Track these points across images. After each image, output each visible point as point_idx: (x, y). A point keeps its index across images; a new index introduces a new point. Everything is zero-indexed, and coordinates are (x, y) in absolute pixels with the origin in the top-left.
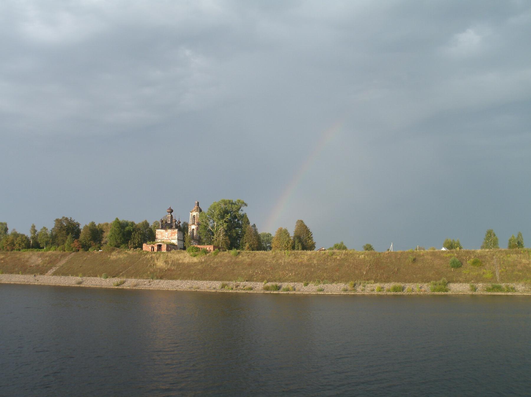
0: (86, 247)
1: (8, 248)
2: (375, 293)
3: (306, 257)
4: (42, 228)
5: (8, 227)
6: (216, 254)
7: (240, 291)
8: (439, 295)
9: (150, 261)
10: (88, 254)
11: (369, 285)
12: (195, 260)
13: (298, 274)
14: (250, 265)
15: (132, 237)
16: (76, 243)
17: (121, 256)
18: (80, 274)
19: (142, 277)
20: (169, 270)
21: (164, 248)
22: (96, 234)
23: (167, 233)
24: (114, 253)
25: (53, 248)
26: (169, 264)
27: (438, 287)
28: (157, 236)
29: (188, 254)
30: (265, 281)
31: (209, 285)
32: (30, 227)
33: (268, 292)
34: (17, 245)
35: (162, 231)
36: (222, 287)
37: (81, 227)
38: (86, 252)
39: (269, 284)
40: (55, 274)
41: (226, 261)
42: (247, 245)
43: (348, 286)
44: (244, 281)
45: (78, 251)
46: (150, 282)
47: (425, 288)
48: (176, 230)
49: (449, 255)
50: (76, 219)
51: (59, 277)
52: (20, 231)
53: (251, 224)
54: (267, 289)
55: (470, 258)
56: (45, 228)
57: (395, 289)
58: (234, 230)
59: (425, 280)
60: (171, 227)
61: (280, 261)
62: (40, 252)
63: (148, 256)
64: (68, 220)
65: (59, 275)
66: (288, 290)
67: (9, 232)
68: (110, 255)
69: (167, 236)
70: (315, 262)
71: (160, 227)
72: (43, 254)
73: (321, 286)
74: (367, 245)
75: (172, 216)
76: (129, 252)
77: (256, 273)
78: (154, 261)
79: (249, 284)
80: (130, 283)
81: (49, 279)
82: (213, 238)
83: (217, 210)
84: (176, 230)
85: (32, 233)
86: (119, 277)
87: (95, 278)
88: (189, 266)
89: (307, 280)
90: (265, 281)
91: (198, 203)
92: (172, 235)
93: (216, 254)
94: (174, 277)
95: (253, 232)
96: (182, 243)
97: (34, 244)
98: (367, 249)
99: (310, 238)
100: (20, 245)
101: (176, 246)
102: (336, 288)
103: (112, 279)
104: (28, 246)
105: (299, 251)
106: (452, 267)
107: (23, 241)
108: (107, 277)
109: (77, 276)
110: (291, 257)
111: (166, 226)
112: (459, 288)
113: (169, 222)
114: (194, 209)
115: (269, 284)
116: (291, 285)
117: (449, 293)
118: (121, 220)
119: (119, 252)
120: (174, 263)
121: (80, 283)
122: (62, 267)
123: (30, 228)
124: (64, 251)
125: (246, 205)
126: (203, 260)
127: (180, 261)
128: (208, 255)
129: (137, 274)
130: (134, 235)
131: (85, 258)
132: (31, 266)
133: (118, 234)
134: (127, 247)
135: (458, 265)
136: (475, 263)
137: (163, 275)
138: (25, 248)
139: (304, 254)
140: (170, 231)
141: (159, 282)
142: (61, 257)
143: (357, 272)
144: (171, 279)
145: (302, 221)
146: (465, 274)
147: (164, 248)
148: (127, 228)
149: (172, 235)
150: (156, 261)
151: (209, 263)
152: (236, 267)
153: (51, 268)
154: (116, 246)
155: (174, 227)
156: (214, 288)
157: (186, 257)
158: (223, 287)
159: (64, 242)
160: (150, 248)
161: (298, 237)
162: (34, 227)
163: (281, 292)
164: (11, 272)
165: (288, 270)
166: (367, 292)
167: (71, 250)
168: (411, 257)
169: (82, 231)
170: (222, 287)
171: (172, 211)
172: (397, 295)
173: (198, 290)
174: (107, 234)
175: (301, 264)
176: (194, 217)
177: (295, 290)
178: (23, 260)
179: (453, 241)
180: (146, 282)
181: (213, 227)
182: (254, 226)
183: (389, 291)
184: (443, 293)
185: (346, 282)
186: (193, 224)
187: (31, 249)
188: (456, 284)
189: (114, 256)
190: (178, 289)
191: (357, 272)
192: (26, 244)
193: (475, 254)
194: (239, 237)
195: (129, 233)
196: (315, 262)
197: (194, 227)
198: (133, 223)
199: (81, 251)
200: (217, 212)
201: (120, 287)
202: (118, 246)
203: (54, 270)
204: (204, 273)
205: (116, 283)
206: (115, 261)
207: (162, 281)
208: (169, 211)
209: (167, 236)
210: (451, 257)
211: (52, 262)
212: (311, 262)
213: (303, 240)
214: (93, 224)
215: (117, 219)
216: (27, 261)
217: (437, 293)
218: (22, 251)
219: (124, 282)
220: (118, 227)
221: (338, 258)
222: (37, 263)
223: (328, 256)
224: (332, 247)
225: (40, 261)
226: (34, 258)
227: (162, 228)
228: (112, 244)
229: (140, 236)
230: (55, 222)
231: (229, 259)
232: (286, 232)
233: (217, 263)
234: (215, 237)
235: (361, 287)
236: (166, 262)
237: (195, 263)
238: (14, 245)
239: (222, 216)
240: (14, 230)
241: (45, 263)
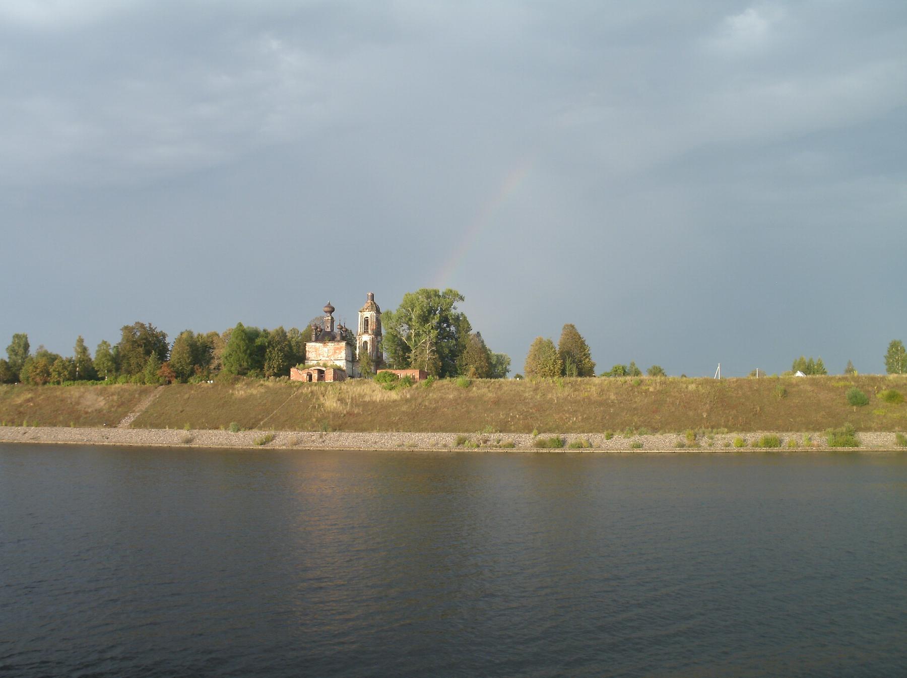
0: (183, 376)
1: (38, 379)
2: (734, 449)
3: (594, 389)
4: (100, 342)
5: (30, 341)
6: (429, 385)
7: (494, 450)
8: (843, 453)
9: (310, 400)
10: (191, 389)
11: (719, 436)
12: (394, 395)
13: (588, 418)
14: (497, 402)
15: (267, 357)
16: (166, 370)
17: (254, 391)
18: (187, 426)
19: (303, 429)
20: (349, 414)
21: (329, 376)
22: (199, 353)
23: (326, 349)
24: (238, 386)
25: (122, 379)
26: (346, 404)
27: (841, 440)
28: (308, 355)
29: (378, 386)
30: (535, 431)
31: (433, 440)
32: (75, 342)
33: (545, 451)
34: (55, 375)
35: (318, 345)
36: (459, 444)
37: (170, 340)
38: (185, 385)
39: (543, 437)
40: (137, 424)
41: (451, 397)
42: (472, 369)
43: (683, 438)
44: (496, 431)
45: (170, 382)
46: (321, 437)
47: (818, 441)
48: (343, 344)
49: (842, 383)
50: (159, 327)
51: (147, 432)
52: (52, 349)
53: (473, 332)
54: (541, 444)
55: (879, 389)
56: (105, 343)
57: (768, 443)
58: (447, 345)
59: (811, 426)
60: (333, 339)
61: (550, 396)
62: (99, 387)
63: (305, 390)
64: (145, 328)
65: (145, 426)
66: (580, 446)
67: (33, 351)
68: (233, 389)
69: (325, 355)
70: (613, 397)
71: (313, 339)
72: (105, 389)
73: (636, 438)
74: (654, 368)
75: (332, 318)
76: (267, 383)
77: (513, 418)
78: (318, 399)
79: (507, 438)
80: (284, 439)
81: (125, 435)
82: (409, 357)
83: (418, 308)
84: (343, 344)
85: (78, 353)
86: (260, 429)
87: (215, 431)
88: (384, 407)
89: (609, 427)
90: (535, 431)
91: (373, 296)
92: (335, 352)
93: (429, 385)
94: (346, 426)
95: (480, 345)
96: (350, 365)
97: (85, 372)
98: (655, 374)
99: (587, 356)
100: (59, 374)
101: (344, 371)
102: (664, 443)
103: (247, 432)
104: (74, 377)
105: (573, 379)
106: (854, 404)
107: (65, 368)
108: (239, 430)
109: (181, 428)
110: (566, 389)
111: (324, 336)
112: (873, 441)
113: (329, 330)
115: (543, 437)
116: (583, 437)
117: (862, 448)
118: (245, 326)
119: (247, 384)
120: (355, 402)
121: (188, 441)
122: (146, 412)
123: (74, 343)
124: (144, 383)
125: (462, 299)
126: (408, 396)
127: (367, 399)
128: (414, 386)
129: (291, 423)
130: (268, 354)
131: (186, 396)
132: (87, 413)
133: (245, 351)
134: (262, 374)
135: (860, 401)
136: (892, 397)
137: (341, 423)
138: (68, 380)
139: (587, 384)
140: (331, 345)
141: (339, 436)
142: (140, 394)
143: (691, 413)
144: (356, 430)
145: (572, 326)
146: (878, 416)
147: (329, 376)
148: (258, 341)
149: (335, 352)
150: (322, 398)
151: (420, 400)
152: (472, 407)
153: (125, 415)
154: (239, 374)
155: (338, 338)
156: (445, 446)
157: (374, 391)
158: (461, 442)
159: (140, 368)
160: (305, 375)
161: (565, 354)
162: (81, 341)
163: (567, 450)
164: (52, 422)
165: (568, 411)
166: (719, 448)
167: (157, 381)
168: (781, 388)
169: (170, 347)
170: (459, 444)
171: (333, 310)
172: (773, 453)
173: (416, 450)
174: (220, 352)
175: (589, 402)
176: (366, 321)
177: (591, 446)
178: (69, 401)
179: (811, 360)
180: (316, 436)
181: (409, 338)
182: (478, 334)
183: (756, 445)
184: (851, 449)
185: (678, 431)
186: (366, 332)
187: (80, 381)
188: (869, 434)
189: (241, 391)
190: (376, 447)
191: (691, 413)
192: (70, 373)
193: (887, 382)
194: (454, 354)
195: (262, 349)
196: (613, 397)
197: (367, 338)
198: (282, 334)
200: (417, 311)
201: (269, 447)
202: (243, 373)
203: (132, 417)
204: (417, 418)
205: (258, 440)
206: (245, 400)
207: (345, 434)
208: (327, 309)
209: (325, 355)
210: (846, 387)
211: (125, 405)
212: (604, 397)
213: (573, 359)
214: (190, 334)
215: (240, 325)
216: (78, 403)
217: (840, 449)
218: (62, 385)
219: (274, 437)
220: (244, 340)
221: (651, 389)
222: (97, 406)
223: (633, 387)
224: (609, 371)
225: (101, 403)
226: (90, 397)
227: (317, 340)
228: (233, 369)
229: (281, 354)
230: (121, 332)
231: (456, 393)
232: (550, 344)
233: (437, 402)
234: (412, 355)
235: (706, 439)
236: (341, 400)
237: (395, 401)
238: (49, 374)
239: (424, 319)
240: (41, 347)
241: (113, 406)
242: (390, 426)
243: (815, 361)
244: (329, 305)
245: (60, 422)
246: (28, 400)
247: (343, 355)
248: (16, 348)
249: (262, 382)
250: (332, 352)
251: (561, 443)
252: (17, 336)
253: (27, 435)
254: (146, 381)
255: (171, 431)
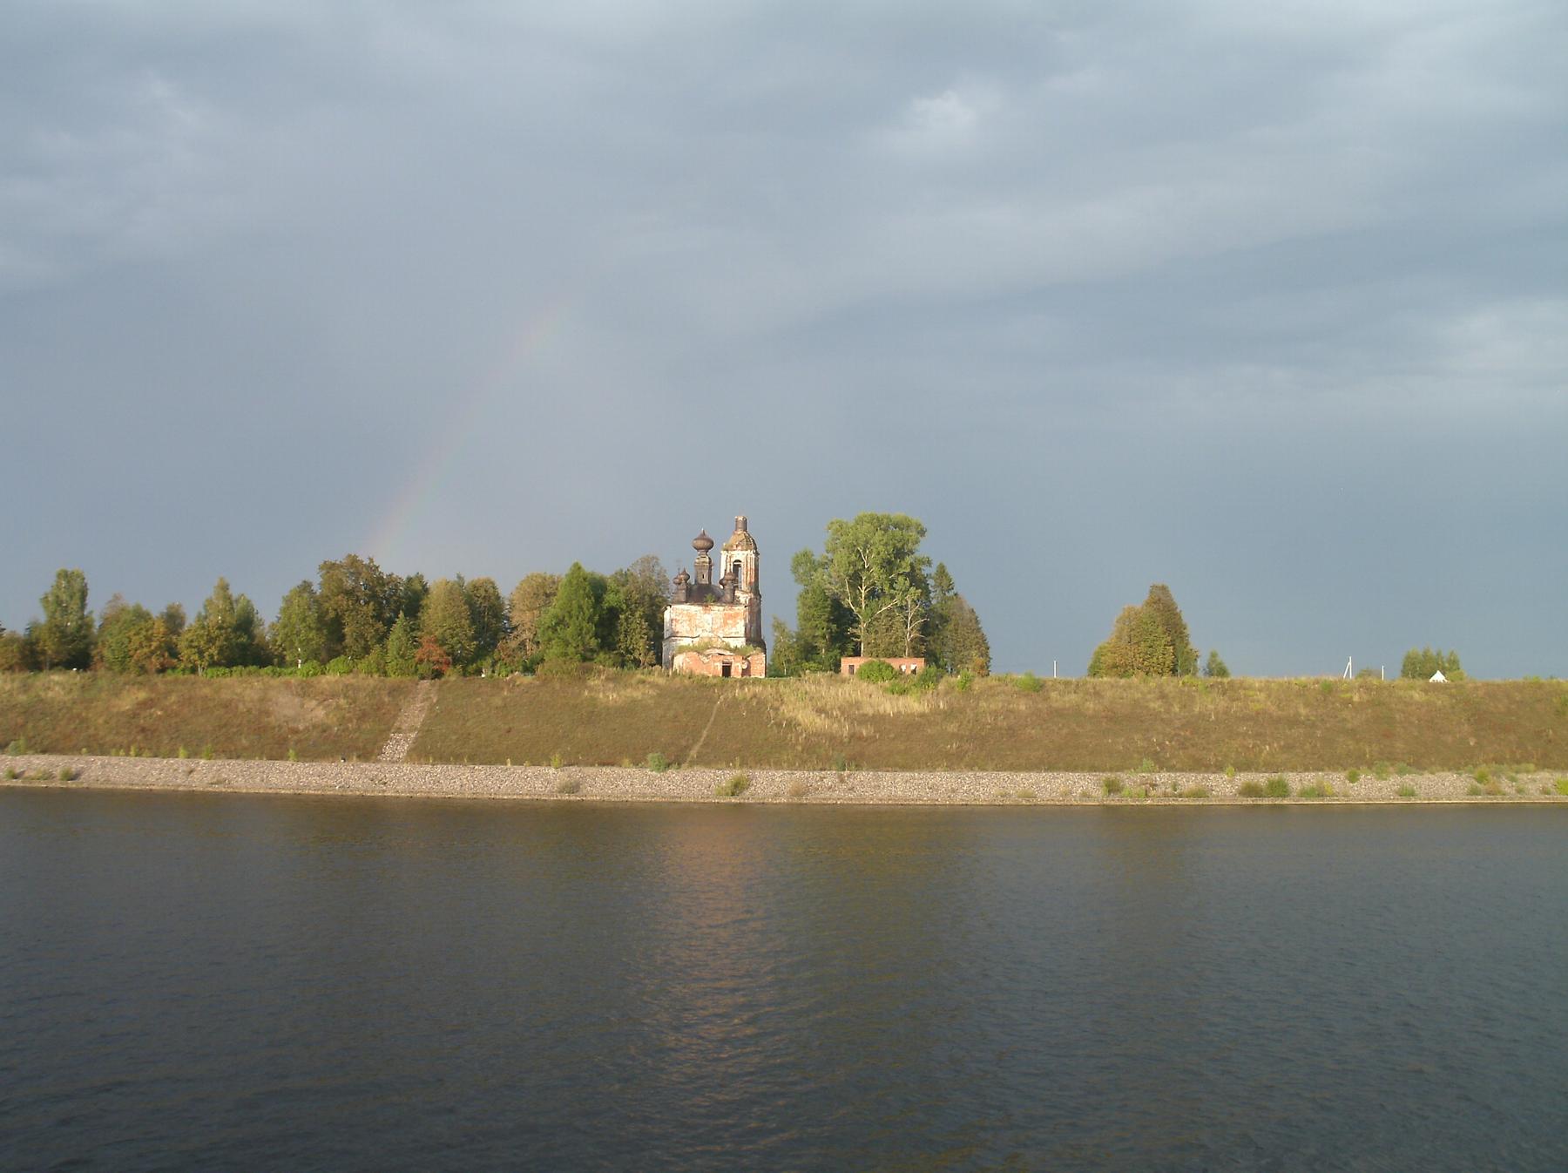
0: (467, 662)
22: (485, 623)
23: (708, 617)
54: (1250, 790)
71: (683, 598)
76: (651, 679)
81: (399, 775)
88: (910, 726)
91: (745, 522)
92: (726, 623)
94: (749, 758)
102: (1445, 787)
114: (733, 540)
116: (1310, 779)
118: (588, 569)
121: (574, 788)
130: (616, 622)
132: (295, 731)
133: (590, 620)
149: (726, 623)
180: (830, 777)
195: (614, 613)
199: (452, 675)
208: (700, 543)
215: (577, 567)
217: (1479, 799)
225: (318, 713)
226: (284, 696)
238: (174, 653)
242: (309, 752)
243: (1433, 652)
244: (703, 537)
245: (245, 749)
246: (146, 704)
247: (740, 628)
248: (64, 597)
249: (639, 676)
250: (719, 622)
251: (1280, 789)
252: (65, 575)
253: (195, 775)
254: (389, 668)
255: (519, 769)
